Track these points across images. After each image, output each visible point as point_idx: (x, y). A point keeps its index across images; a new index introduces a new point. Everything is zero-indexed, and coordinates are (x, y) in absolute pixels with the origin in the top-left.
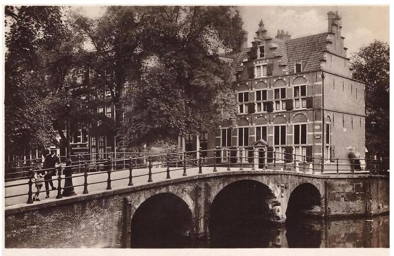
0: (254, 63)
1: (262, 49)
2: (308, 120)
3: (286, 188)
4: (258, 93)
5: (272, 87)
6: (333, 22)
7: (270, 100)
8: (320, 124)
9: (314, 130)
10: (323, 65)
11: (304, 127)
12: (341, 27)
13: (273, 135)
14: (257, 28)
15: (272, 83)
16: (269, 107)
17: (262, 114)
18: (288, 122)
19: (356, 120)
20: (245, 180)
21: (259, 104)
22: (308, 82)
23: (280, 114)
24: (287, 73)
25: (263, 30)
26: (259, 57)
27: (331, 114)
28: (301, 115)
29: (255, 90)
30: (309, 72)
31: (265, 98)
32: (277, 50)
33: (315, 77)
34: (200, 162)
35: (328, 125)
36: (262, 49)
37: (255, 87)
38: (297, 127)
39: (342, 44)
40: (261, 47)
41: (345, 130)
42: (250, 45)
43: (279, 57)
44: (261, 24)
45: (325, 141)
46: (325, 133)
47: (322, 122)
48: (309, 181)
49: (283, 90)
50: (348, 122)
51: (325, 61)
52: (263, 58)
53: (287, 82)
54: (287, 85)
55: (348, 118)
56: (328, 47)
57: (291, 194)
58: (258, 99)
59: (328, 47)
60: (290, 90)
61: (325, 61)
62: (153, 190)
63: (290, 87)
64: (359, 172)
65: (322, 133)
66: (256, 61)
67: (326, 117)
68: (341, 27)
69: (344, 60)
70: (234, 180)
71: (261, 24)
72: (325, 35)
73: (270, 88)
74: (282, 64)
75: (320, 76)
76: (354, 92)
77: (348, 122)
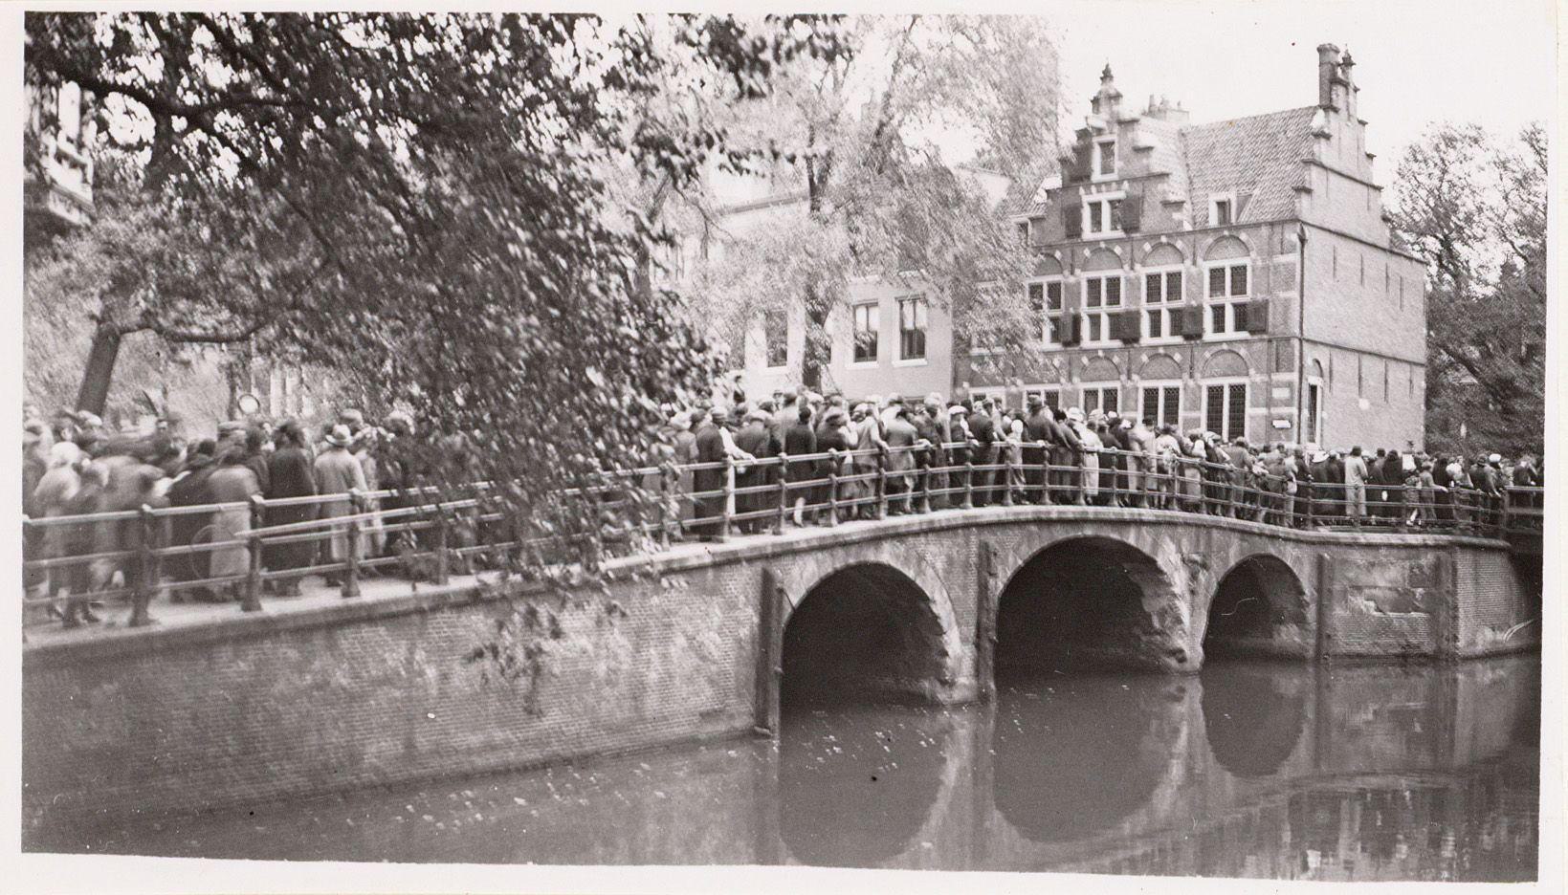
0: (1082, 191)
1: (1107, 146)
2: (1252, 371)
3: (1204, 566)
4: (1094, 284)
5: (1138, 266)
6: (1334, 74)
7: (1133, 308)
8: (1290, 385)
9: (1270, 403)
10: (1303, 204)
11: (1238, 392)
12: (1356, 90)
13: (1249, 411)
14: (1095, 87)
15: (1138, 255)
16: (1125, 329)
17: (1166, 346)
18: (1186, 376)
19: (1399, 374)
20: (1086, 538)
21: (1095, 320)
22: (1253, 254)
23: (1225, 347)
24: (1188, 227)
25: (1112, 92)
26: (1097, 176)
27: (1323, 355)
28: (1229, 356)
29: (1083, 277)
30: (1257, 225)
31: (1114, 299)
32: (1153, 154)
33: (1276, 239)
34: (1298, 507)
35: (1313, 389)
36: (1107, 146)
37: (1144, 264)
38: (1215, 394)
39: (1359, 142)
40: (1103, 145)
41: (1364, 404)
42: (1069, 139)
43: (1163, 176)
44: (1107, 76)
45: (1304, 436)
46: (1306, 413)
47: (1295, 377)
48: (1272, 551)
49: (1114, 284)
50: (1372, 381)
51: (1309, 191)
52: (1108, 177)
53: (1188, 253)
54: (1188, 262)
55: (1373, 368)
56: (1323, 151)
57: (1221, 585)
58: (1094, 300)
59: (1323, 151)
60: (1133, 284)
61: (1309, 191)
62: (840, 552)
63: (1196, 272)
64: (1485, 541)
65: (1295, 410)
66: (1087, 188)
67: (1309, 362)
68: (1356, 90)
69: (1365, 189)
70: (1060, 534)
71: (1107, 76)
72: (1311, 111)
73: (1194, 263)
74: (1172, 198)
75: (1295, 238)
76: (1394, 288)
77: (1372, 381)
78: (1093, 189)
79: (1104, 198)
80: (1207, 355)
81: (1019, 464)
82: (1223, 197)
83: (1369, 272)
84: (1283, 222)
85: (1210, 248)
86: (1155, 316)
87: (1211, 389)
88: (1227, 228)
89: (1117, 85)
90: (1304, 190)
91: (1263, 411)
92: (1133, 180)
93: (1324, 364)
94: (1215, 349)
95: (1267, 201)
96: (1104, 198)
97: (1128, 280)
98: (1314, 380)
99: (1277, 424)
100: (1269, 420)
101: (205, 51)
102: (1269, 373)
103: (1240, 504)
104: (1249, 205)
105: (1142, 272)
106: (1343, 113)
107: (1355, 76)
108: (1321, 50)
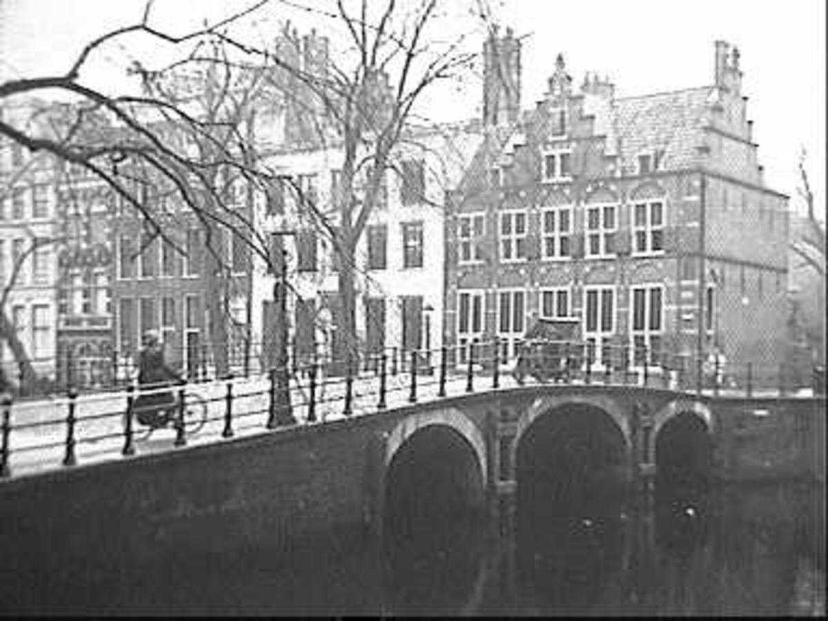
9: (679, 301)
11: (518, 295)
13: (664, 307)
41: (745, 301)
47: (697, 282)
55: (751, 274)
67: (707, 271)
72: (710, 89)
75: (697, 183)
78: (549, 147)
79: (557, 152)
80: (634, 267)
81: (544, 154)
82: (644, 152)
83: (750, 206)
84: (690, 172)
85: (637, 190)
86: (595, 238)
87: (589, 292)
88: (649, 171)
89: (569, 69)
90: (705, 149)
91: (674, 308)
92: (578, 140)
93: (717, 272)
94: (639, 263)
95: (679, 154)
96: (557, 152)
97: (575, 212)
98: (710, 284)
99: (686, 317)
100: (679, 313)
101: (292, 210)
102: (679, 280)
103: (599, 343)
104: (663, 160)
105: (586, 207)
106: (733, 93)
107: (743, 65)
108: (717, 44)
